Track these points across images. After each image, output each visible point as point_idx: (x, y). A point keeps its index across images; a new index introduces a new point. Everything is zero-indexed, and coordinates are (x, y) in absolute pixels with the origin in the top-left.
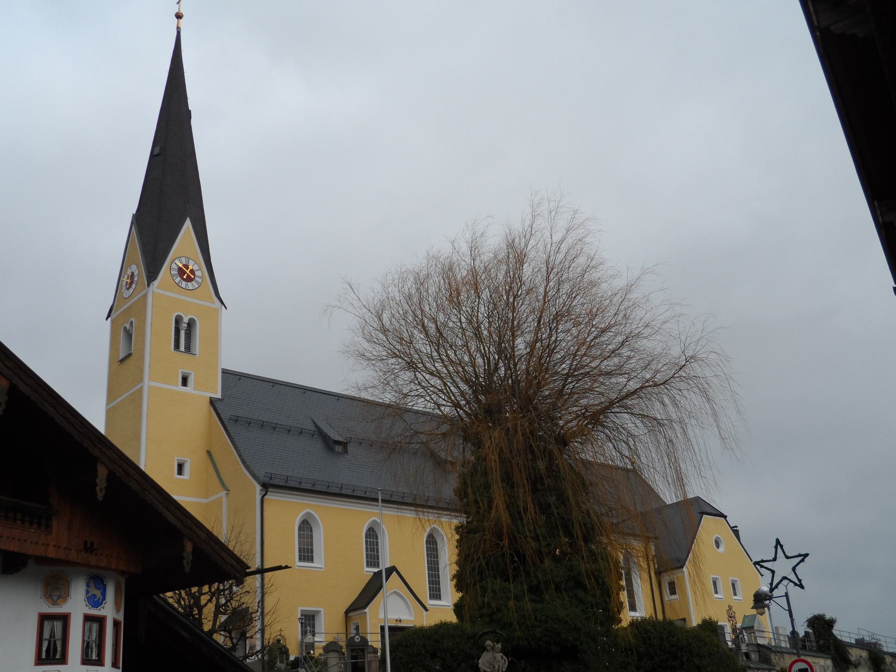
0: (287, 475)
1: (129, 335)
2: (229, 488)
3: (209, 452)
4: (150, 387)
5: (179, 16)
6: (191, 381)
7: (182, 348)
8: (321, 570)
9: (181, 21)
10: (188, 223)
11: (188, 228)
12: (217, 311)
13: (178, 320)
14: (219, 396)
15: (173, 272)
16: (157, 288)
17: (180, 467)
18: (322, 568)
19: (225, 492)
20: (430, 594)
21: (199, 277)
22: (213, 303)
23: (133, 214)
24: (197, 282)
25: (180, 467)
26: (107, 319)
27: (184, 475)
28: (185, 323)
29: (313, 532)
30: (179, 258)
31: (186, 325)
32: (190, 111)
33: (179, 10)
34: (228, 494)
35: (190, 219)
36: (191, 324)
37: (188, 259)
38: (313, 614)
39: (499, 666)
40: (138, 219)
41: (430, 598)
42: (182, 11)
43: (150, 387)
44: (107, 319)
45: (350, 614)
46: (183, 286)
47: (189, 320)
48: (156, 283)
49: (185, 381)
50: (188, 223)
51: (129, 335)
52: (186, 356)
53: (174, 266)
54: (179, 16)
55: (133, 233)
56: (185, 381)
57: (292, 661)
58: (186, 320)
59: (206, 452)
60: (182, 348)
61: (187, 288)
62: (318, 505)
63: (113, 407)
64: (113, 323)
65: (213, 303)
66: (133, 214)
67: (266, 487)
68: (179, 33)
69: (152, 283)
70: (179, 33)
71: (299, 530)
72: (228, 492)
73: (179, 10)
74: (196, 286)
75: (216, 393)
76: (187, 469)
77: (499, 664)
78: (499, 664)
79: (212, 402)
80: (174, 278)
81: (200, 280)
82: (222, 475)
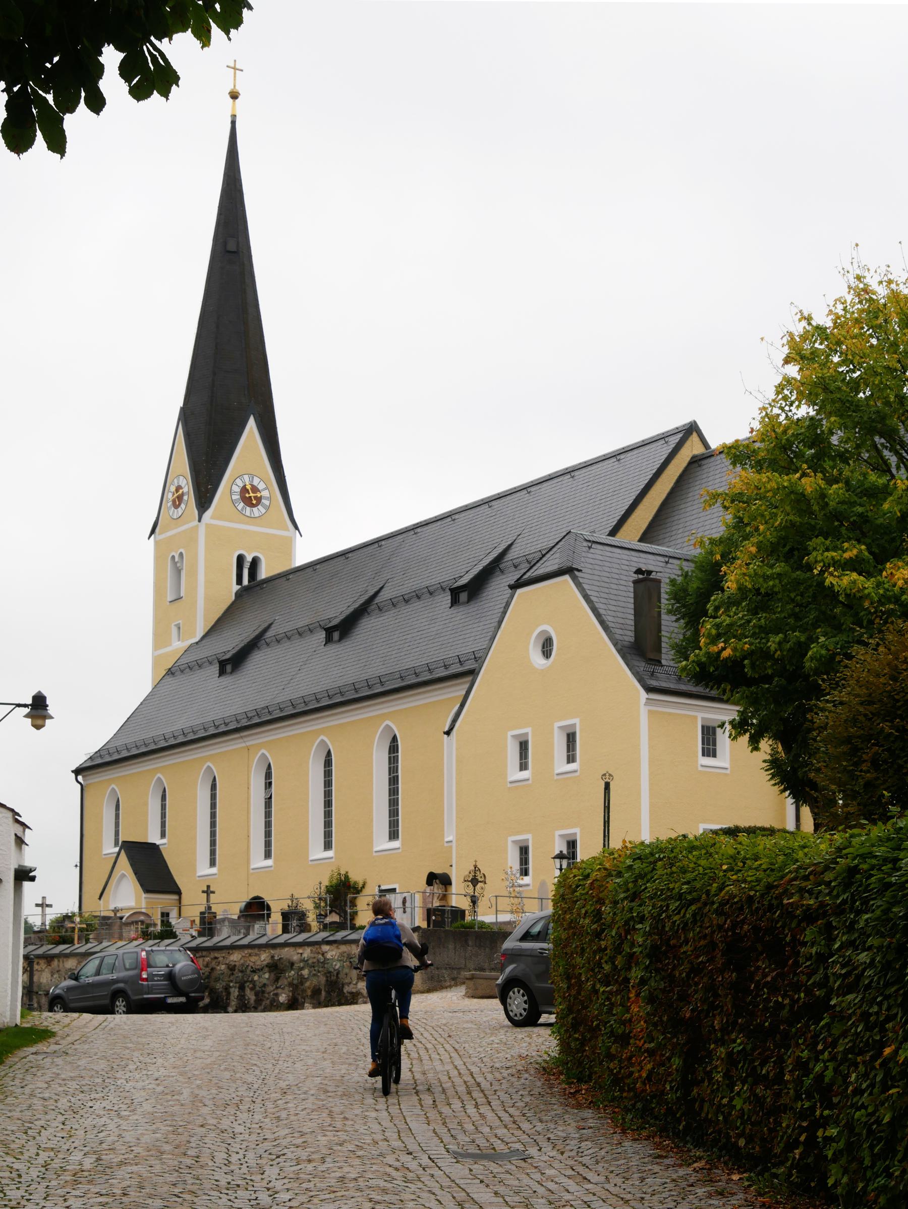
0: (457, 654)
5: (234, 96)
8: (576, 774)
9: (230, 87)
10: (251, 424)
11: (251, 428)
13: (240, 559)
15: (234, 497)
18: (726, 769)
20: (703, 749)
21: (266, 498)
24: (264, 506)
26: (149, 538)
33: (235, 86)
41: (703, 755)
42: (239, 88)
44: (149, 538)
46: (248, 514)
50: (251, 424)
55: (180, 435)
57: (827, 1083)
58: (249, 559)
61: (253, 516)
62: (395, 711)
64: (157, 543)
68: (233, 123)
70: (233, 123)
73: (235, 86)
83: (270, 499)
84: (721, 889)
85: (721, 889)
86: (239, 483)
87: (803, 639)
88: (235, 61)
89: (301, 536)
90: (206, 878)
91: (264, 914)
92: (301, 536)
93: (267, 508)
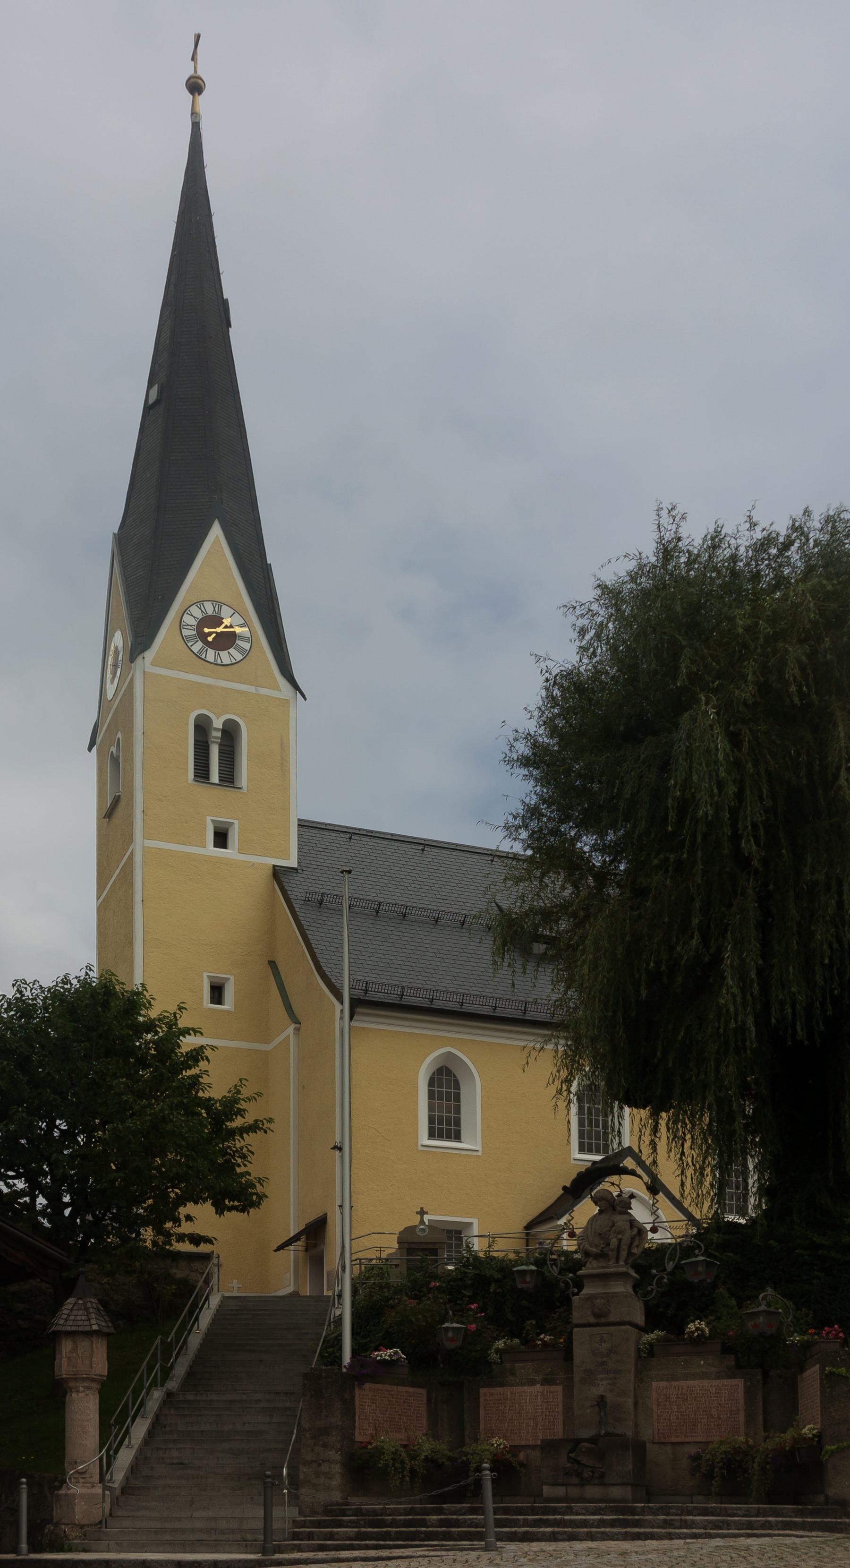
1: (115, 760)
2: (301, 1021)
3: (273, 964)
4: (146, 851)
6: (234, 837)
7: (215, 777)
9: (201, 99)
10: (216, 532)
11: (217, 541)
12: (286, 703)
13: (202, 727)
14: (293, 863)
15: (186, 632)
16: (152, 664)
17: (217, 992)
18: (477, 1151)
19: (293, 1026)
22: (278, 689)
23: (114, 534)
24: (240, 650)
25: (217, 992)
26: (90, 749)
27: (224, 1005)
28: (217, 729)
29: (462, 1089)
30: (199, 603)
31: (219, 734)
32: (225, 303)
34: (297, 1030)
35: (220, 523)
36: (230, 733)
37: (220, 604)
38: (458, 1228)
39: (620, 1240)
40: (122, 540)
43: (146, 851)
44: (90, 749)
45: (534, 1231)
47: (224, 724)
48: (150, 655)
49: (221, 838)
51: (115, 760)
52: (227, 793)
53: (187, 619)
54: (195, 87)
56: (221, 838)
58: (218, 723)
59: (267, 962)
60: (215, 777)
63: (104, 900)
65: (278, 689)
66: (114, 534)
67: (358, 1004)
68: (196, 127)
69: (140, 657)
70: (196, 127)
71: (431, 1083)
72: (297, 1025)
74: (239, 657)
75: (286, 856)
76: (229, 994)
77: (620, 1236)
78: (620, 1236)
79: (277, 873)
80: (189, 644)
81: (247, 646)
82: (291, 999)
83: (250, 640)
84: (793, 1006)
85: (793, 1006)
86: (196, 611)
87: (755, 863)
88: (198, 38)
89: (305, 699)
90: (469, 1153)
91: (584, 1127)
92: (305, 699)
93: (246, 654)
